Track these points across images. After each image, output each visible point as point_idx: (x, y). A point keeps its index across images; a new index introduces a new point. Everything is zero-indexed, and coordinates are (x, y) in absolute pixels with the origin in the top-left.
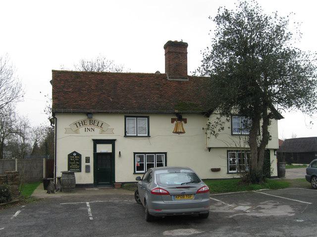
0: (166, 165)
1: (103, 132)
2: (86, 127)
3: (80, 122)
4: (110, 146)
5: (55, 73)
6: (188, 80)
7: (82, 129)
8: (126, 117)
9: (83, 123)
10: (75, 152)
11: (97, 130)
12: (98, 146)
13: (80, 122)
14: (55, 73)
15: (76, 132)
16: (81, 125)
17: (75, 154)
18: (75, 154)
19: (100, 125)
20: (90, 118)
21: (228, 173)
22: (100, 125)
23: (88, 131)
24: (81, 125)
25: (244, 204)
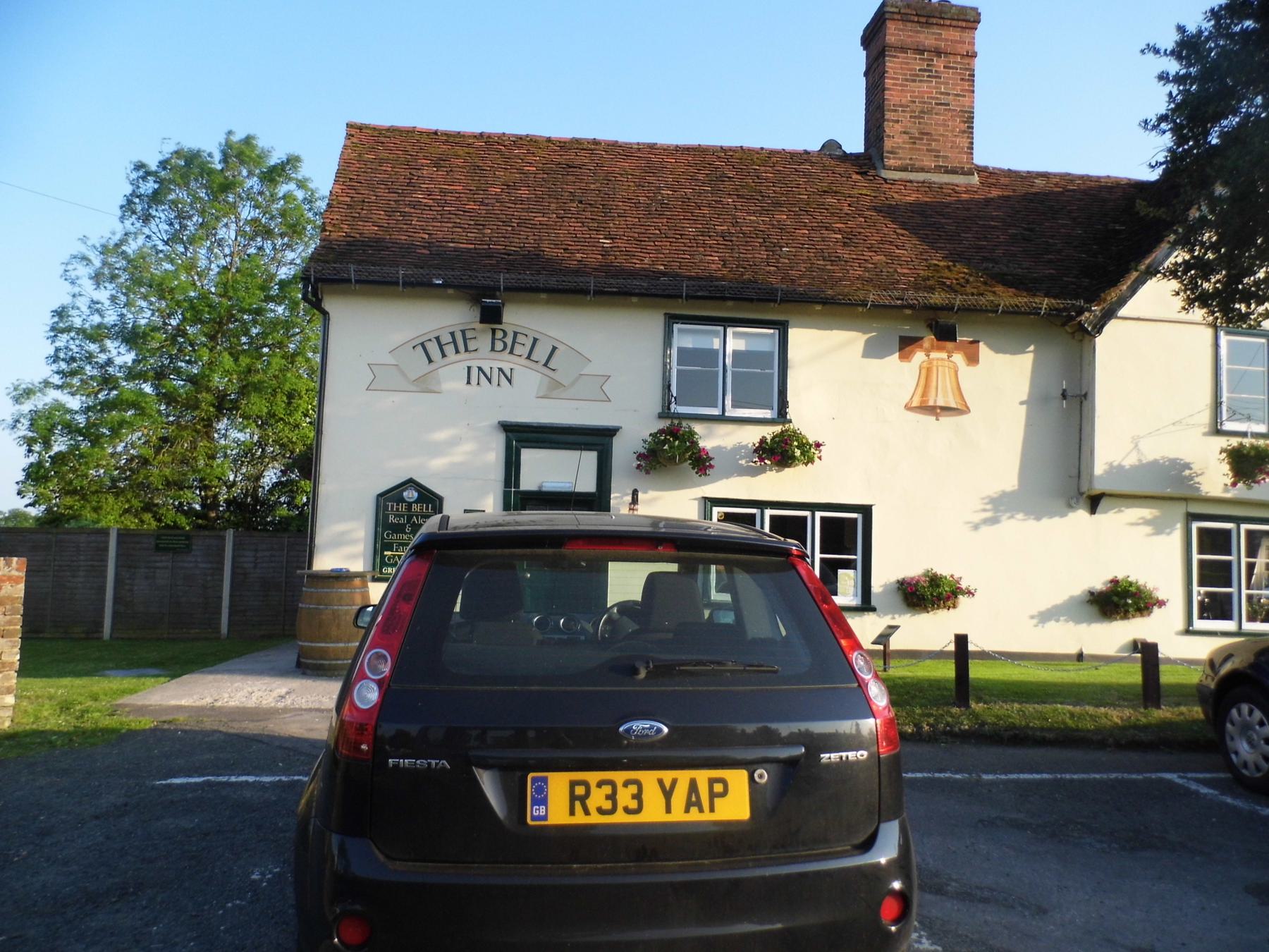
0: (469, 368)
1: (554, 389)
2: (475, 364)
3: (446, 338)
4: (589, 459)
5: (356, 131)
6: (975, 179)
7: (451, 376)
8: (672, 319)
9: (460, 341)
10: (411, 483)
11: (528, 378)
12: (587, 484)
13: (446, 338)
14: (356, 131)
15: (424, 385)
16: (449, 349)
17: (411, 495)
18: (411, 495)
19: (541, 353)
20: (491, 316)
21: (1189, 631)
22: (541, 353)
23: (504, 381)
24: (449, 349)
25: (1056, 663)
